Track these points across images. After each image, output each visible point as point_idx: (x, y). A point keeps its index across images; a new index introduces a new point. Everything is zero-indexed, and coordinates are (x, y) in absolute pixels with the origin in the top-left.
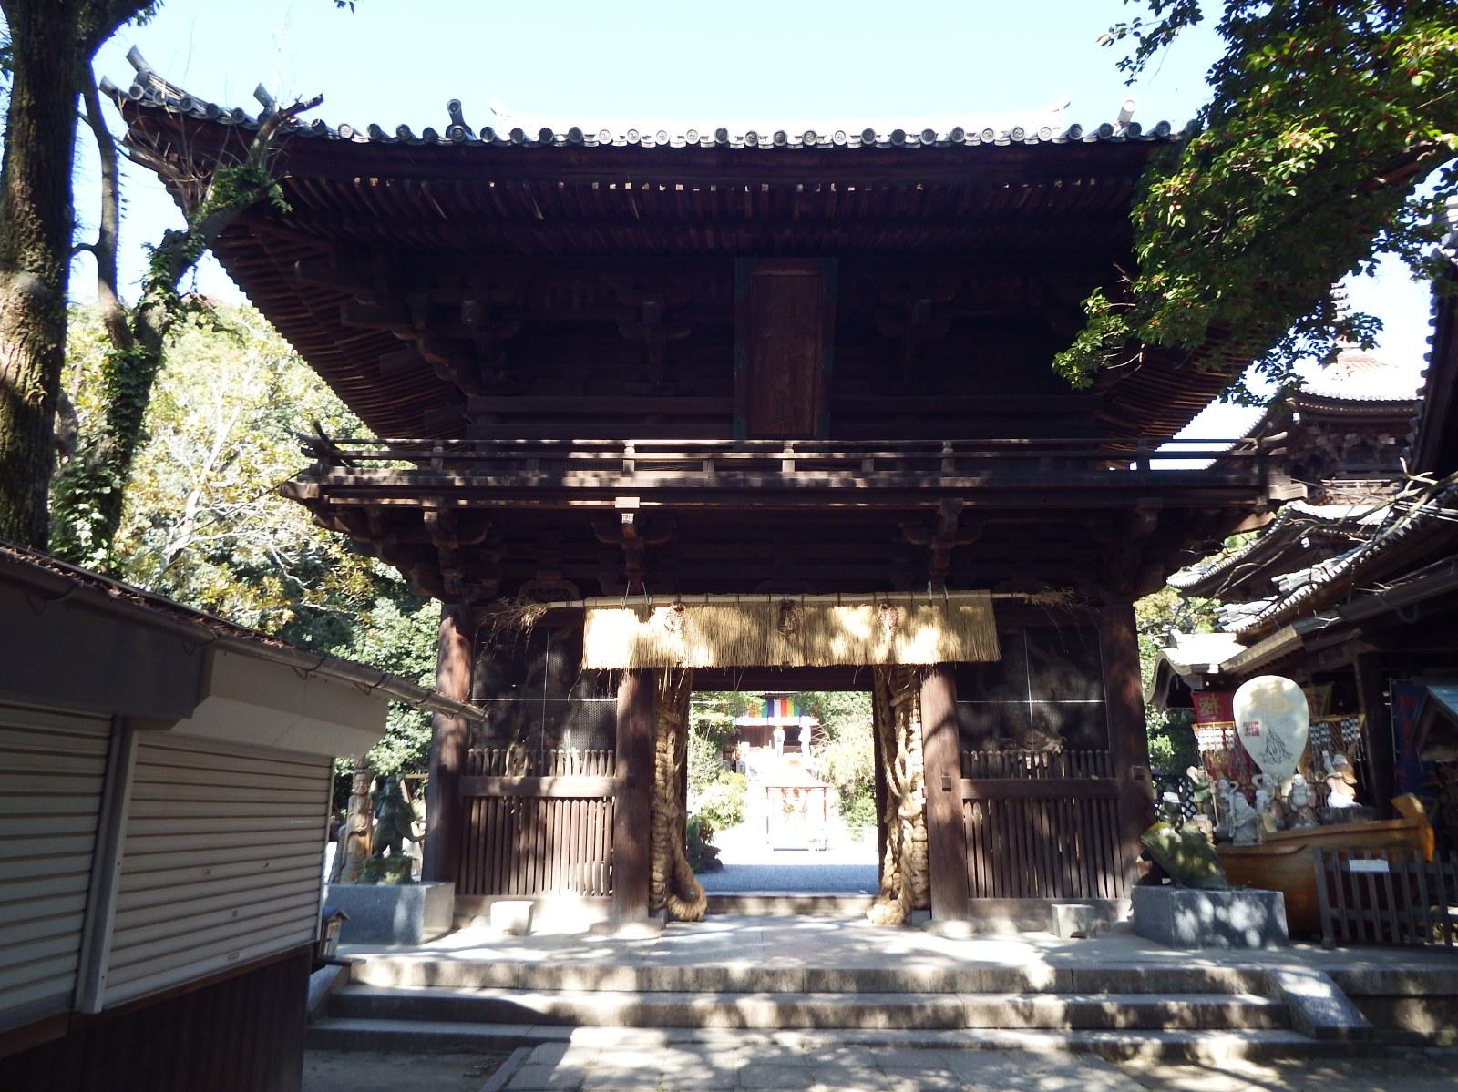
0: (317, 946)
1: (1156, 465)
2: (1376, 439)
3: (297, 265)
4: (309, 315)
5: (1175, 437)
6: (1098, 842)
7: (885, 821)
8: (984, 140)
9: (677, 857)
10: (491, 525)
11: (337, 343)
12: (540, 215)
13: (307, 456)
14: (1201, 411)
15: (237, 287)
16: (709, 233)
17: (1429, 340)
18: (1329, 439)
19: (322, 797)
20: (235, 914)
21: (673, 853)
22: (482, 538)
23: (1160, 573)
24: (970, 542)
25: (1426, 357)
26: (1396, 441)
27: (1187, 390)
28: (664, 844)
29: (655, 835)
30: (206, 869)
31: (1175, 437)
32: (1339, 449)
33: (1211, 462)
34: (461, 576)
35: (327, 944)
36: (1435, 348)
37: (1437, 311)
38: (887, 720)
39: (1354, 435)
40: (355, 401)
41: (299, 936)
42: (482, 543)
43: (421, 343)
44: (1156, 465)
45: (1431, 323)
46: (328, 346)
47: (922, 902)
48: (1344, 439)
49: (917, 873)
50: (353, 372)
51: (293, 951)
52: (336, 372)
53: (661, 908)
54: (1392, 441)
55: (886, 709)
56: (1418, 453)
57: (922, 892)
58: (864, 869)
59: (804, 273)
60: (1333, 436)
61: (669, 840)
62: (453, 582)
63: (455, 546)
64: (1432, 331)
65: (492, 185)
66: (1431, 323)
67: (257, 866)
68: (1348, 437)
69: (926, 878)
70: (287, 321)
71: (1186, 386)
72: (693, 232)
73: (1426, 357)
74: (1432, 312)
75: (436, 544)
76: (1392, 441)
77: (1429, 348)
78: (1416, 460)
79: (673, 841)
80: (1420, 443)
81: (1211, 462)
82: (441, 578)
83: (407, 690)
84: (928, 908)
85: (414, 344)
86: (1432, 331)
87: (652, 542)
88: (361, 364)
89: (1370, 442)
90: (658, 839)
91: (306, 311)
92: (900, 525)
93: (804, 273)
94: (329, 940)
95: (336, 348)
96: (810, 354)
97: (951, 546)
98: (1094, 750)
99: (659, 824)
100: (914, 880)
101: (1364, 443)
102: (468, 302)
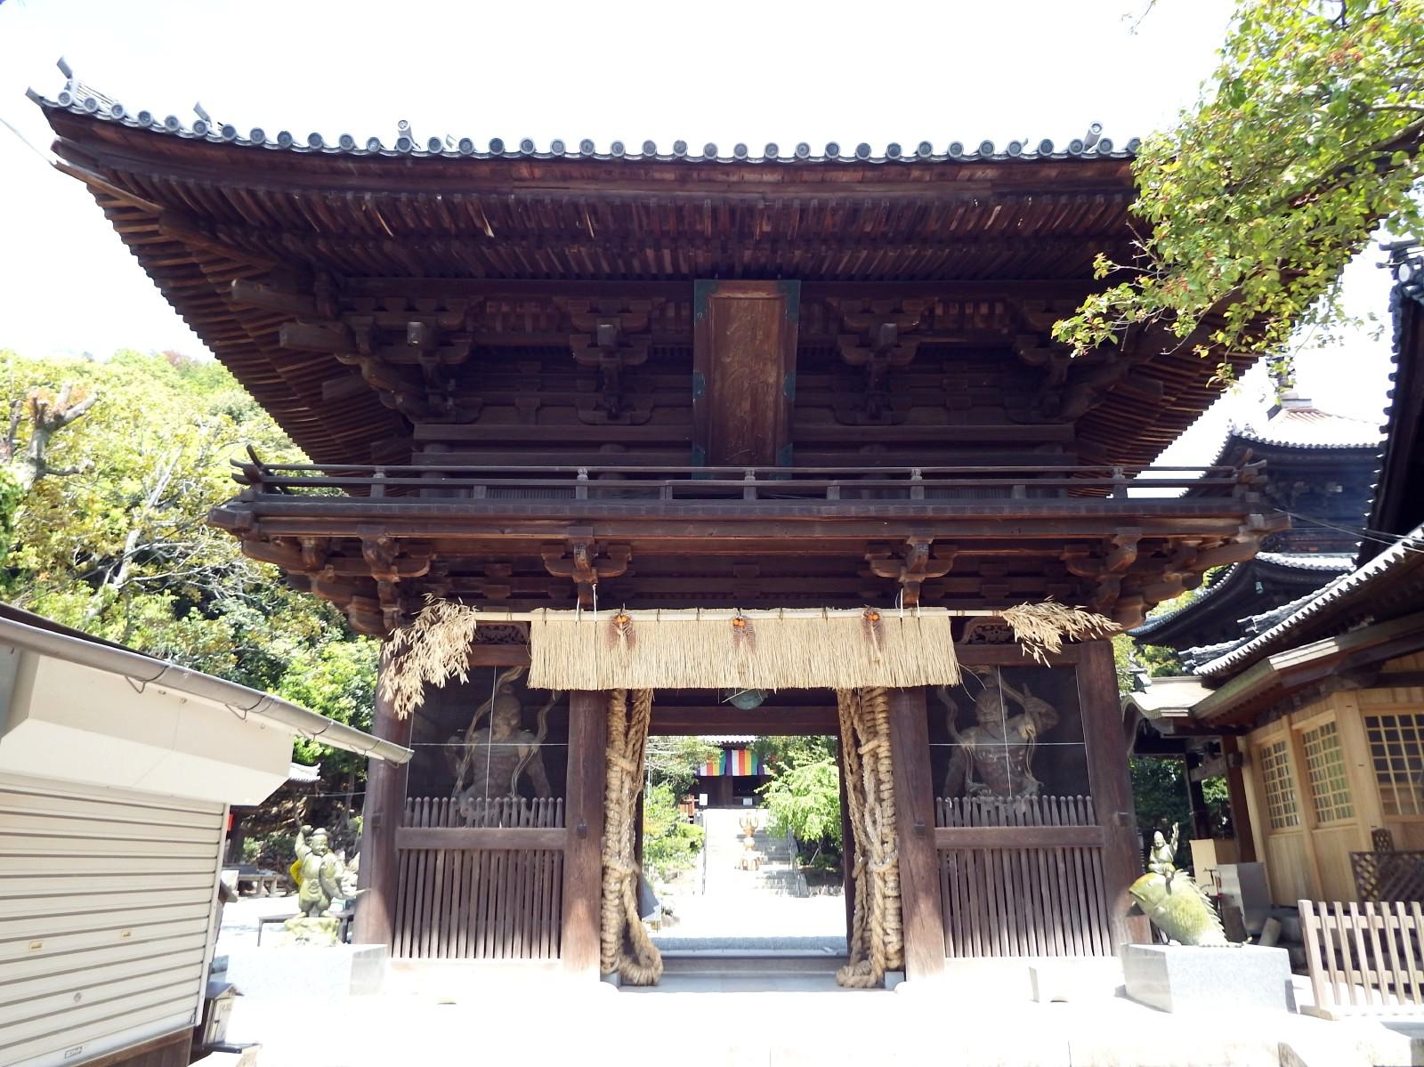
0: (199, 1032)
1: (1133, 493)
2: (1324, 487)
3: (234, 283)
4: (251, 340)
5: (1152, 465)
6: (1082, 896)
7: (854, 875)
8: (951, 155)
9: (629, 917)
10: (434, 557)
11: (279, 370)
12: (490, 233)
13: (238, 482)
14: (1250, 367)
15: (173, 309)
16: (667, 253)
17: (1391, 377)
18: (1277, 488)
19: (212, 851)
20: (78, 997)
21: (625, 912)
22: (425, 571)
23: (1140, 607)
24: (941, 575)
25: (1389, 394)
26: (1343, 489)
27: (1154, 426)
28: (617, 901)
29: (606, 893)
30: (126, 931)
31: (1152, 465)
32: (1288, 497)
33: (1183, 490)
34: (402, 612)
35: (215, 1025)
36: (1397, 385)
37: (1399, 348)
38: (855, 767)
39: (1302, 483)
40: (299, 434)
41: (177, 1016)
42: (425, 575)
43: (365, 369)
44: (1133, 493)
45: (1393, 360)
46: (270, 374)
47: (895, 963)
48: (1292, 488)
49: (889, 931)
50: (297, 403)
51: (159, 1042)
52: (279, 402)
53: (614, 972)
54: (1340, 490)
55: (853, 754)
56: (1384, 490)
57: (896, 953)
58: (832, 942)
59: (764, 295)
60: (1281, 484)
61: (622, 897)
62: (393, 618)
63: (396, 579)
64: (1394, 368)
65: (439, 198)
66: (1393, 360)
67: (116, 936)
68: (1297, 484)
69: (899, 937)
70: (226, 347)
71: (1153, 421)
72: (650, 253)
73: (1389, 394)
74: (1394, 349)
75: (375, 577)
76: (1340, 490)
77: (1392, 385)
78: (1382, 498)
79: (626, 899)
80: (1385, 482)
81: (1183, 490)
82: (381, 613)
83: (1414, 892)
84: (902, 969)
85: (358, 368)
86: (1394, 368)
87: (607, 575)
88: (304, 394)
89: (1318, 489)
90: (610, 896)
91: (246, 336)
92: (868, 556)
93: (764, 295)
94: (218, 1022)
95: (279, 377)
96: (771, 380)
97: (920, 579)
98: (1075, 797)
99: (612, 881)
100: (887, 939)
101: (1312, 491)
102: (415, 324)
